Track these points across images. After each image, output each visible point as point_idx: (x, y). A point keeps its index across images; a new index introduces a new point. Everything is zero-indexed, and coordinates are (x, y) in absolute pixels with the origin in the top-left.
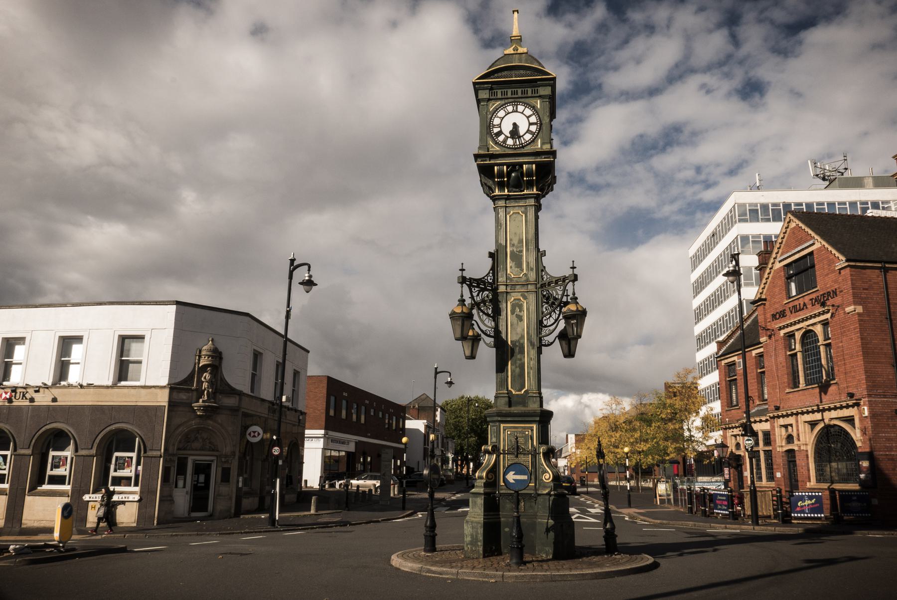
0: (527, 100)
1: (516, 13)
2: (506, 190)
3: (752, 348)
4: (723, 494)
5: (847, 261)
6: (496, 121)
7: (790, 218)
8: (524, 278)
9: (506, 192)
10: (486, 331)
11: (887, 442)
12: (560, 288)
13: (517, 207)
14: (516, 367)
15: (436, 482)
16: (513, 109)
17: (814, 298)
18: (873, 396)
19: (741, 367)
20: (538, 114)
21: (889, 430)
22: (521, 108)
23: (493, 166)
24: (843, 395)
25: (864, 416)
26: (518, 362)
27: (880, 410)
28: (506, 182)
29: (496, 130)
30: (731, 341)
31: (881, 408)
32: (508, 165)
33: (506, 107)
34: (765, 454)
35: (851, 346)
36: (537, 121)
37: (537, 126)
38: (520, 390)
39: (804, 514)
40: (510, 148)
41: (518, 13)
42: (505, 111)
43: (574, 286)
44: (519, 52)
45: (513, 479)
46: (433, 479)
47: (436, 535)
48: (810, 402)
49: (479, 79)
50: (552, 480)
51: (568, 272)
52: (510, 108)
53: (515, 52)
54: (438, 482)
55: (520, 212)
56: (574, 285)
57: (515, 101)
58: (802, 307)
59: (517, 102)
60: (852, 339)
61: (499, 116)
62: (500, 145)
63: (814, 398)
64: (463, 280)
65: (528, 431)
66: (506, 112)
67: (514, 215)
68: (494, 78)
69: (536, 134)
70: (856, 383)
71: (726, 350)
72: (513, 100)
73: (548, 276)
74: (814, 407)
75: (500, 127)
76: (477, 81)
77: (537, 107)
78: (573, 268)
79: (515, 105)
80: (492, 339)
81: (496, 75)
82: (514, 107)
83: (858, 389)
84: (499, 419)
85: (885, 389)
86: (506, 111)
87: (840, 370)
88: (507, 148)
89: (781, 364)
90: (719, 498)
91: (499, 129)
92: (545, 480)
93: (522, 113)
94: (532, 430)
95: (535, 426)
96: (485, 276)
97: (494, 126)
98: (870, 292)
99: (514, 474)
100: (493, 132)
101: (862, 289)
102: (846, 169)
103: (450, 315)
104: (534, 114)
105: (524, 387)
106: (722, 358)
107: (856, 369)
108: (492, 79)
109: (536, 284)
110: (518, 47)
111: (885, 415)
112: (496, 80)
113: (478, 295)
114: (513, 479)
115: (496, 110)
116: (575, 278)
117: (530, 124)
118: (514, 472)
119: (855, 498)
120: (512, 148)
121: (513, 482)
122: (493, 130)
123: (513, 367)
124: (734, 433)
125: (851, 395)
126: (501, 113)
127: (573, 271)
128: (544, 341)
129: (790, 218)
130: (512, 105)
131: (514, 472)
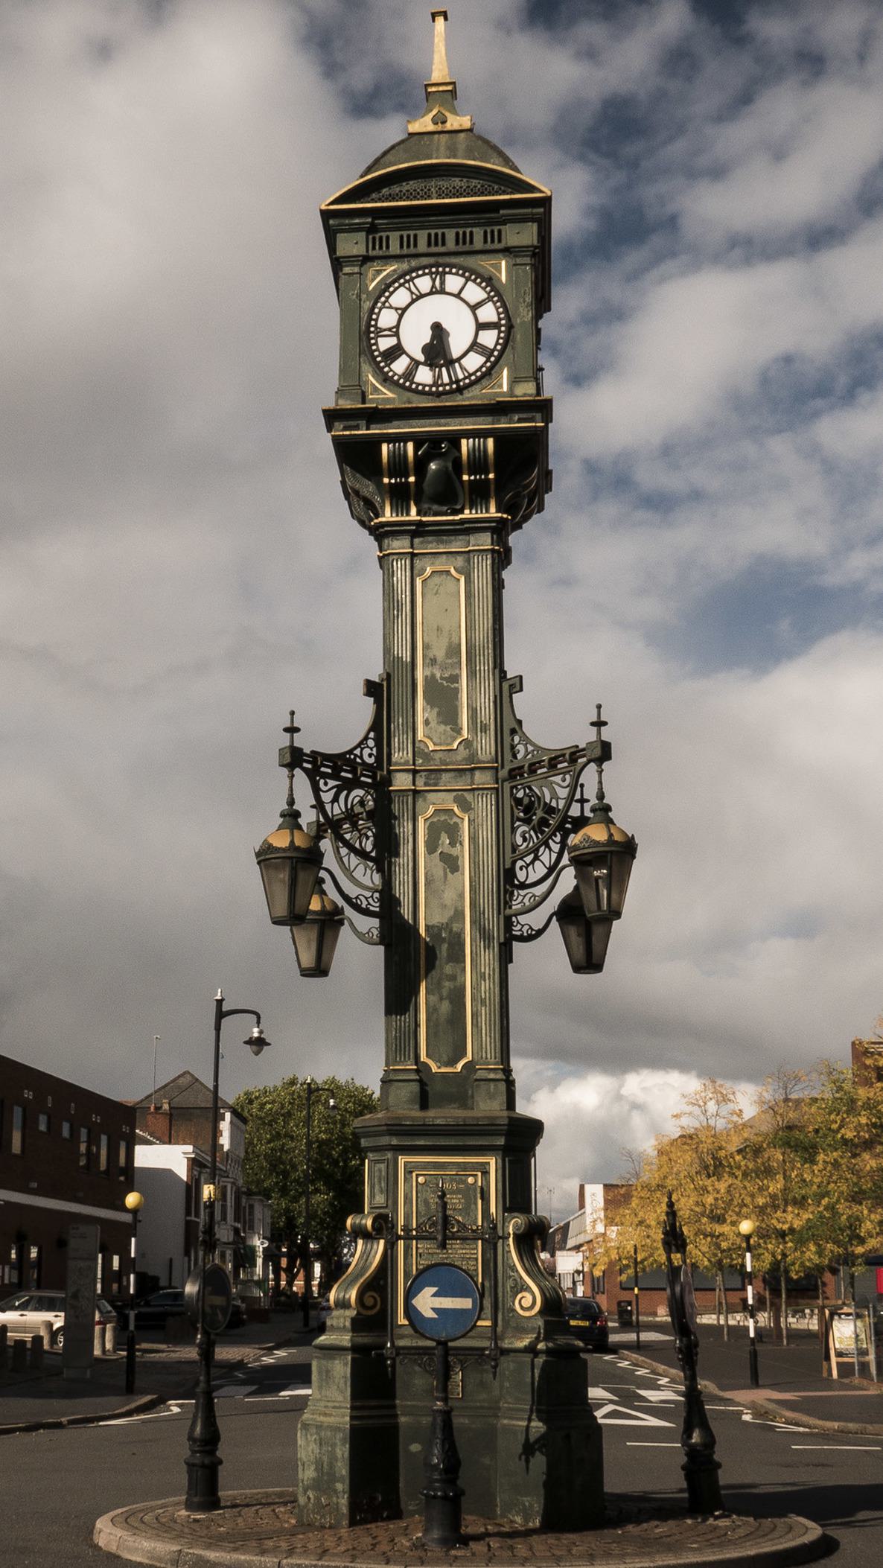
1: (440, 20)
6: (386, 319)
10: (357, 898)
12: (564, 780)
14: (441, 999)
16: (433, 286)
20: (501, 300)
22: (453, 282)
23: (375, 442)
29: (385, 344)
32: (418, 440)
33: (412, 279)
36: (500, 319)
37: (500, 332)
38: (452, 1062)
40: (423, 393)
41: (446, 19)
42: (409, 289)
44: (448, 126)
45: (433, 1309)
47: (221, 1462)
49: (337, 201)
50: (540, 1312)
51: (585, 736)
52: (424, 283)
53: (439, 127)
56: (600, 772)
57: (439, 263)
59: (445, 266)
62: (396, 383)
64: (294, 758)
66: (412, 293)
67: (436, 579)
68: (380, 200)
69: (496, 353)
72: (431, 260)
73: (530, 748)
75: (397, 335)
77: (500, 280)
78: (599, 724)
79: (437, 273)
80: (375, 922)
81: (385, 191)
82: (434, 280)
84: (395, 1142)
86: (413, 289)
88: (416, 391)
91: (393, 341)
92: (521, 1312)
93: (458, 296)
94: (486, 1173)
95: (493, 1162)
96: (355, 748)
97: (379, 332)
99: (434, 1295)
100: (378, 350)
103: (258, 855)
104: (489, 299)
105: (464, 1054)
109: (496, 768)
110: (447, 114)
113: (335, 799)
114: (433, 1309)
115: (386, 288)
116: (604, 753)
117: (481, 326)
118: (435, 1289)
120: (430, 393)
122: (376, 344)
123: (433, 998)
126: (400, 298)
127: (599, 733)
128: (519, 927)
130: (431, 273)
131: (435, 1289)
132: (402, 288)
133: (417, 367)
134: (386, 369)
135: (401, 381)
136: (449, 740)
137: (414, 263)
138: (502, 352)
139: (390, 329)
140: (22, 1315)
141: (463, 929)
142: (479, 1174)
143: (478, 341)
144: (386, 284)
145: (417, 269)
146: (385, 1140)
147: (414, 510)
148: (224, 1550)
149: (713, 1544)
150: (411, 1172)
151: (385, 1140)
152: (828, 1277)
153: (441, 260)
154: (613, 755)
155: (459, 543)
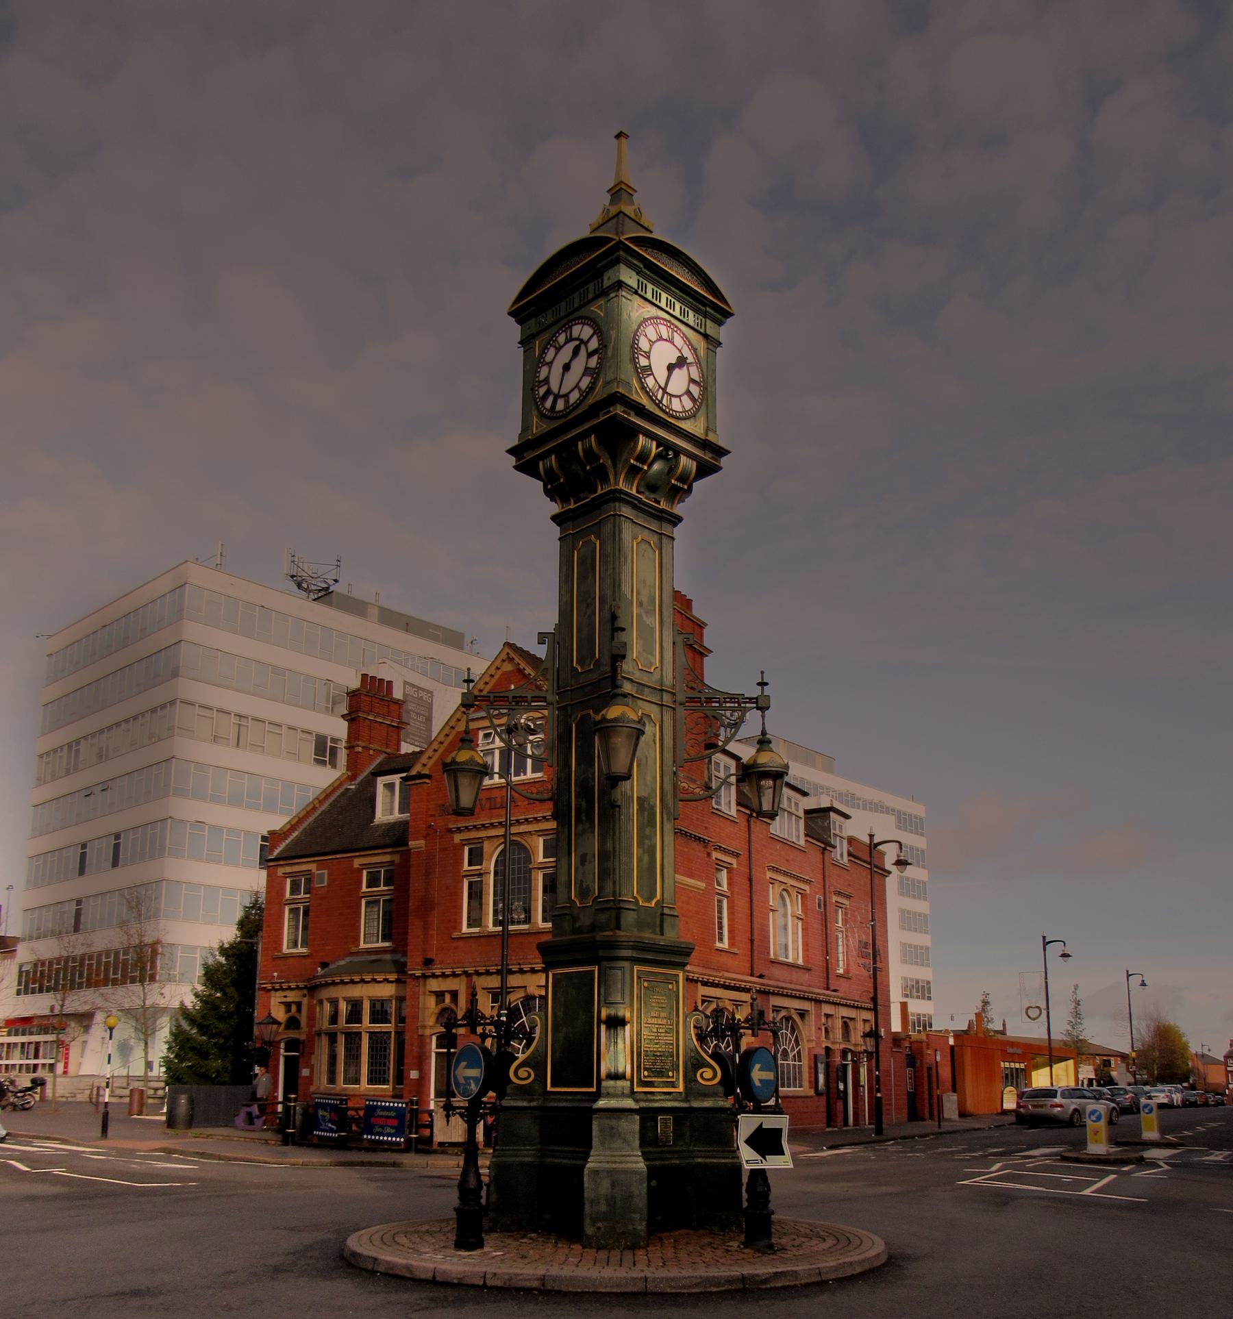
0: (576, 315)
3: (357, 854)
4: (323, 1103)
7: (508, 654)
12: (732, 716)
13: (647, 530)
14: (644, 852)
15: (473, 1086)
19: (323, 883)
26: (647, 841)
34: (370, 1038)
39: (380, 1136)
43: (763, 719)
45: (760, 1081)
46: (466, 1078)
49: (512, 306)
50: (720, 1083)
51: (755, 692)
54: (476, 1085)
56: (763, 717)
67: (644, 546)
71: (282, 852)
75: (648, 358)
78: (762, 684)
89: (447, 888)
90: (379, 1113)
102: (336, 581)
106: (282, 863)
121: (759, 1085)
123: (640, 850)
124: (288, 1000)
127: (762, 689)
130: (563, 331)
132: (651, 327)
139: (645, 352)
140: (285, 997)
141: (656, 804)
148: (827, 1267)
149: (832, 1252)
152: (316, 1038)
154: (112, 847)
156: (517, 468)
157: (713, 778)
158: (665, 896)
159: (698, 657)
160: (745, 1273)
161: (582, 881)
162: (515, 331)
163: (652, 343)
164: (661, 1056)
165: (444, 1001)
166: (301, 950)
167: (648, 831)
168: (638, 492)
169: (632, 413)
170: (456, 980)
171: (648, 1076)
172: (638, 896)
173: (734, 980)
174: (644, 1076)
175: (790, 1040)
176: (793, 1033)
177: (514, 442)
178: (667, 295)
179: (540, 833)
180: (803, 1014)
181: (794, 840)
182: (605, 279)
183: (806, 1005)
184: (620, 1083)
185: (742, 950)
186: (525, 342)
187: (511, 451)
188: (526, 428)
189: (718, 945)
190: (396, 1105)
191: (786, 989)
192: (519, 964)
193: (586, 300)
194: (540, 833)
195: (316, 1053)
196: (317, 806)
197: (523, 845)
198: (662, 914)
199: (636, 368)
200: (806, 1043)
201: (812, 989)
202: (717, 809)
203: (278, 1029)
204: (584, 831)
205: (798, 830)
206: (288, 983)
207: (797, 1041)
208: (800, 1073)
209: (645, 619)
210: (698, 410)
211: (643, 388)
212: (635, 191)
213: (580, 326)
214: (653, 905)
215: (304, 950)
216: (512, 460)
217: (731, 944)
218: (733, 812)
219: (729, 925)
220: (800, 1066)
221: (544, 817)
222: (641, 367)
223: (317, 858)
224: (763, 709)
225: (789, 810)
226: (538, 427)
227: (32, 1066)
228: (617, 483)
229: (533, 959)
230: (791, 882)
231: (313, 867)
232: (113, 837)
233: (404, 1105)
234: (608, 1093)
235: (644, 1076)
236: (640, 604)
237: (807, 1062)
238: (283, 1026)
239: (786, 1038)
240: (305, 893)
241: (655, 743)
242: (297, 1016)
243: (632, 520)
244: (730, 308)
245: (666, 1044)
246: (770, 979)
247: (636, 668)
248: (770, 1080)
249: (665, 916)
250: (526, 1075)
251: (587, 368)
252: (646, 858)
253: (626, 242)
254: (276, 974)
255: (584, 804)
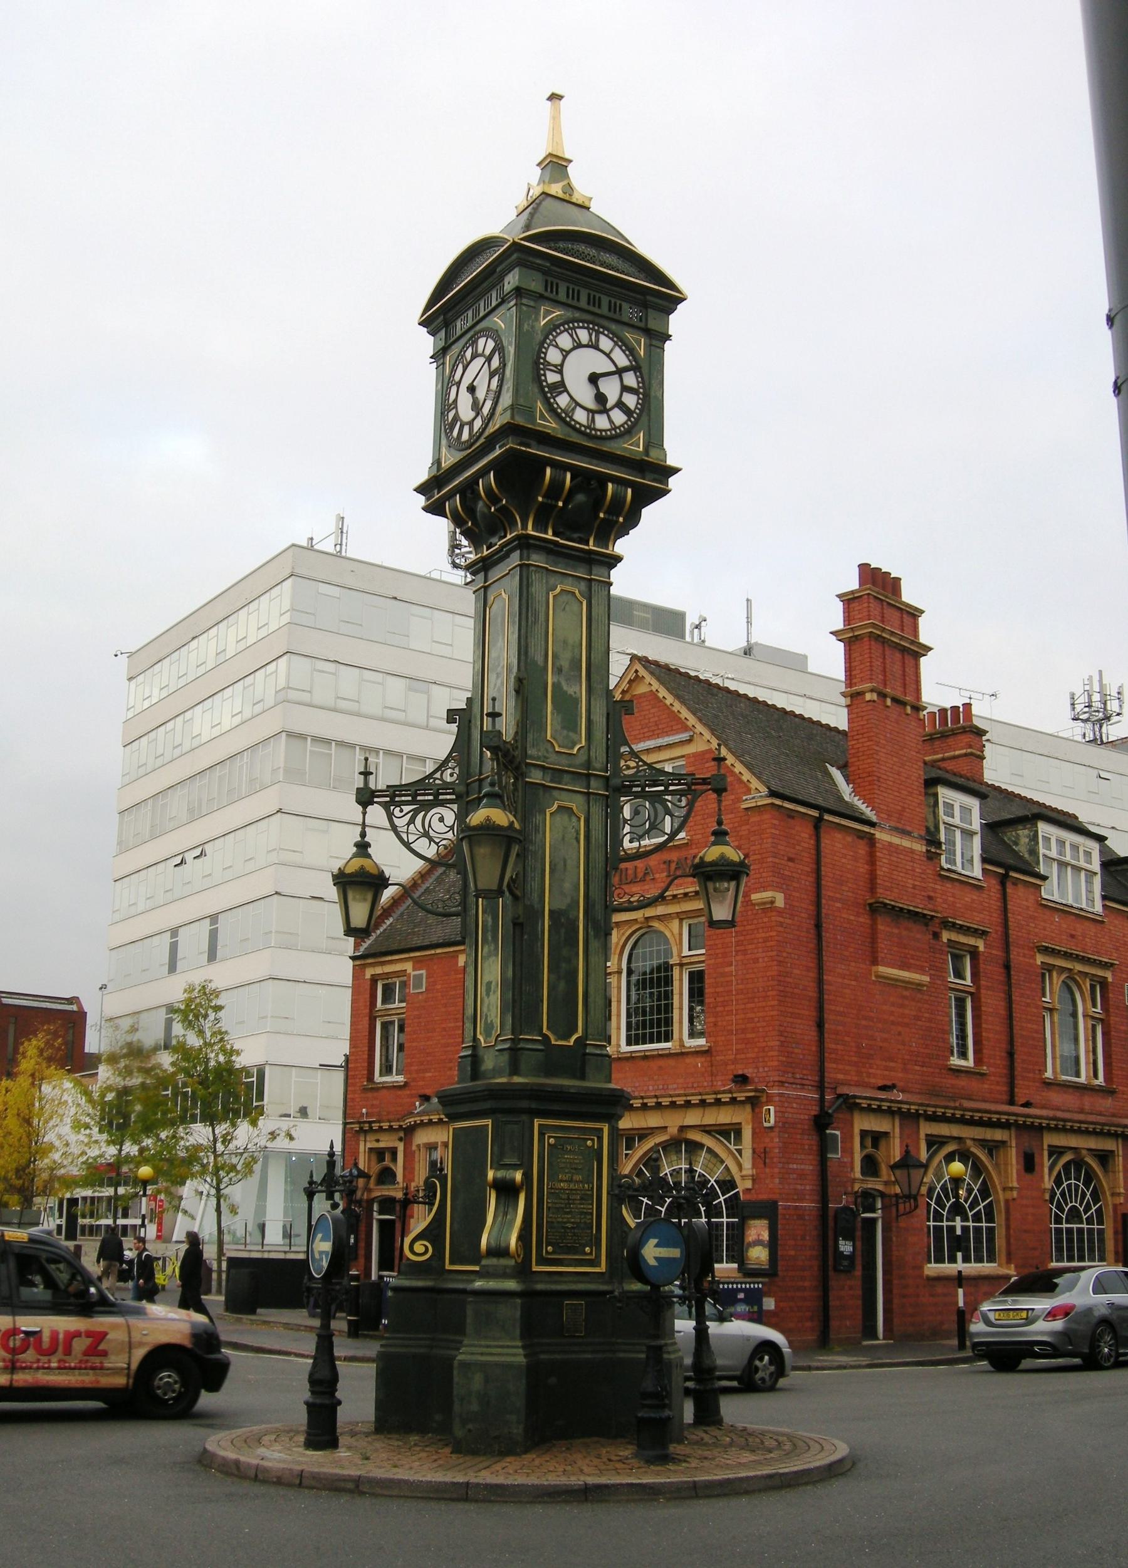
2: (591, 542)
5: (773, 794)
7: (636, 671)
8: (583, 758)
9: (549, 536)
11: (799, 1182)
17: (675, 859)
18: (786, 1085)
21: (803, 1157)
22: (605, 343)
24: (718, 1078)
25: (766, 1125)
26: (564, 965)
27: (795, 1116)
28: (545, 500)
29: (552, 378)
30: (388, 922)
31: (796, 1111)
32: (576, 472)
33: (574, 328)
35: (753, 976)
38: (567, 1037)
40: (578, 431)
42: (571, 336)
45: (656, 1258)
47: (339, 1403)
48: (636, 1087)
49: (422, 316)
55: (577, 592)
57: (598, 322)
58: (640, 875)
59: (600, 326)
60: (756, 961)
61: (561, 345)
62: (558, 416)
63: (646, 1079)
65: (593, 1140)
67: (565, 598)
68: (555, 250)
70: (753, 1055)
74: (650, 1100)
75: (561, 372)
76: (523, 242)
79: (593, 329)
81: (561, 245)
82: (590, 335)
83: (757, 1068)
84: (534, 1106)
85: (805, 1072)
87: (720, 1023)
88: (574, 428)
93: (608, 355)
94: (600, 1139)
98: (798, 866)
99: (657, 1246)
101: (786, 858)
105: (576, 1030)
106: (370, 961)
107: (758, 1025)
108: (550, 248)
111: (799, 1126)
112: (576, 260)
114: (656, 1258)
115: (553, 329)
119: (741, 1296)
121: (655, 1264)
124: (382, 1145)
125: (742, 1080)
126: (565, 341)
129: (636, 671)
130: (588, 328)
132: (566, 333)
133: (575, 408)
134: (637, 411)
135: (633, 419)
136: (570, 745)
137: (577, 315)
138: (568, 424)
139: (555, 366)
140: (378, 1141)
142: (596, 1139)
143: (565, 393)
144: (554, 325)
145: (578, 321)
146: (524, 1104)
147: (550, 532)
150: (544, 1134)
151: (524, 1104)
153: (597, 320)
155: (581, 570)
156: (426, 509)
157: (942, 827)
158: (589, 1031)
159: (909, 660)
160: (242, 1459)
161: (486, 1015)
162: (426, 343)
163: (566, 354)
164: (573, 1228)
165: (384, 1160)
166: (397, 1078)
167: (565, 952)
168: (554, 534)
169: (533, 443)
170: (395, 1136)
171: (553, 1253)
172: (549, 1033)
173: (979, 1111)
174: (547, 1252)
175: (1084, 1195)
176: (1087, 1184)
177: (423, 476)
178: (587, 291)
179: (681, 916)
180: (1104, 1158)
181: (1084, 906)
182: (506, 284)
183: (1109, 1145)
184: (503, 1262)
185: (995, 1066)
186: (439, 356)
187: (422, 489)
188: (437, 462)
189: (955, 1061)
190: (748, 1286)
191: (1069, 1121)
192: (656, 1097)
193: (490, 308)
194: (681, 916)
195: (416, 1216)
196: (419, 882)
197: (662, 932)
198: (585, 1054)
199: (542, 388)
200: (1109, 1198)
201: (1116, 1120)
202: (949, 870)
203: (368, 1183)
204: (489, 955)
205: (1090, 891)
206: (379, 1122)
207: (1096, 1197)
208: (1102, 1241)
209: (565, 688)
210: (634, 425)
211: (553, 410)
212: (570, 161)
213: (485, 339)
214: (572, 1044)
215: (400, 1079)
216: (421, 500)
217: (978, 1060)
218: (977, 871)
219: (975, 1034)
220: (1101, 1232)
221: (686, 895)
222: (548, 386)
223: (412, 955)
224: (720, 791)
225: (1073, 862)
226: (449, 459)
227: (87, 1233)
228: (525, 527)
229: (675, 1089)
230: (1079, 967)
231: (408, 967)
232: (169, 933)
233: (760, 1286)
234: (488, 1273)
235: (547, 1252)
236: (558, 670)
237: (1112, 1225)
238: (372, 1180)
239: (1076, 1191)
240: (401, 1001)
241: (578, 841)
242: (392, 1166)
243: (546, 569)
244: (681, 293)
245: (582, 1213)
246: (1043, 1107)
247: (551, 750)
248: (674, 1259)
249: (587, 1057)
250: (422, 1250)
251: (456, 407)
252: (562, 985)
253: (523, 242)
254: (364, 1110)
255: (490, 919)
